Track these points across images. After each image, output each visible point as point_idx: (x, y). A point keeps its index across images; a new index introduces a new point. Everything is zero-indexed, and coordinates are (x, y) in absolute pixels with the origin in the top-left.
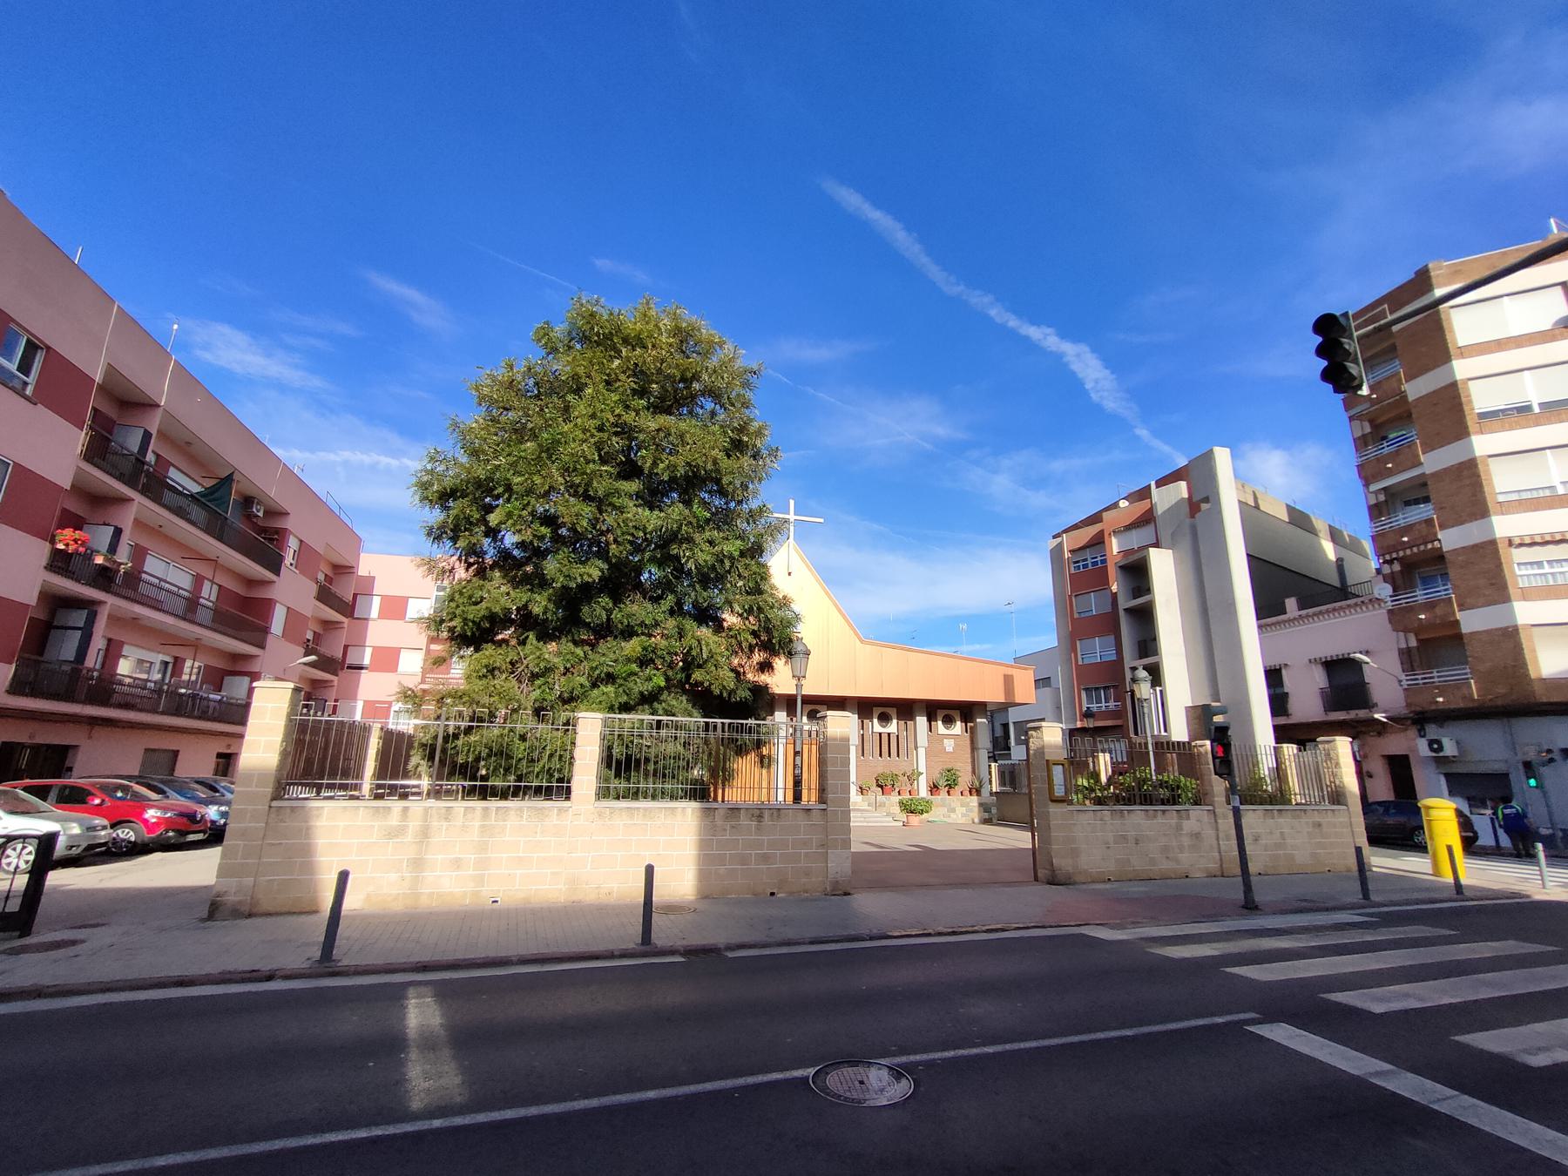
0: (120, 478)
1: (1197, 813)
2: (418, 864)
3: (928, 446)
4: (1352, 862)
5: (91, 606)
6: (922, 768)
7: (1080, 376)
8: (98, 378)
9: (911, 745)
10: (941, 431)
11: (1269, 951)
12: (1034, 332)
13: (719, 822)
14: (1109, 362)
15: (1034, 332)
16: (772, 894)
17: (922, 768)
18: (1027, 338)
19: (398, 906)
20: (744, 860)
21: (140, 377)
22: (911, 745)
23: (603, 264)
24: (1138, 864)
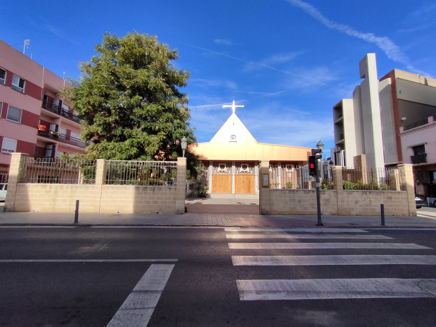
0: (55, 112)
1: (331, 192)
2: (54, 200)
3: (324, 84)
4: (379, 210)
5: (54, 145)
6: (280, 182)
7: (383, 50)
8: (42, 87)
9: (277, 175)
10: (329, 78)
11: (282, 239)
12: (364, 36)
13: (140, 191)
14: (397, 42)
15: (364, 36)
16: (157, 213)
17: (280, 182)
18: (361, 39)
19: (50, 211)
20: (148, 202)
21: (55, 86)
22: (277, 175)
23: (217, 41)
24: (299, 209)
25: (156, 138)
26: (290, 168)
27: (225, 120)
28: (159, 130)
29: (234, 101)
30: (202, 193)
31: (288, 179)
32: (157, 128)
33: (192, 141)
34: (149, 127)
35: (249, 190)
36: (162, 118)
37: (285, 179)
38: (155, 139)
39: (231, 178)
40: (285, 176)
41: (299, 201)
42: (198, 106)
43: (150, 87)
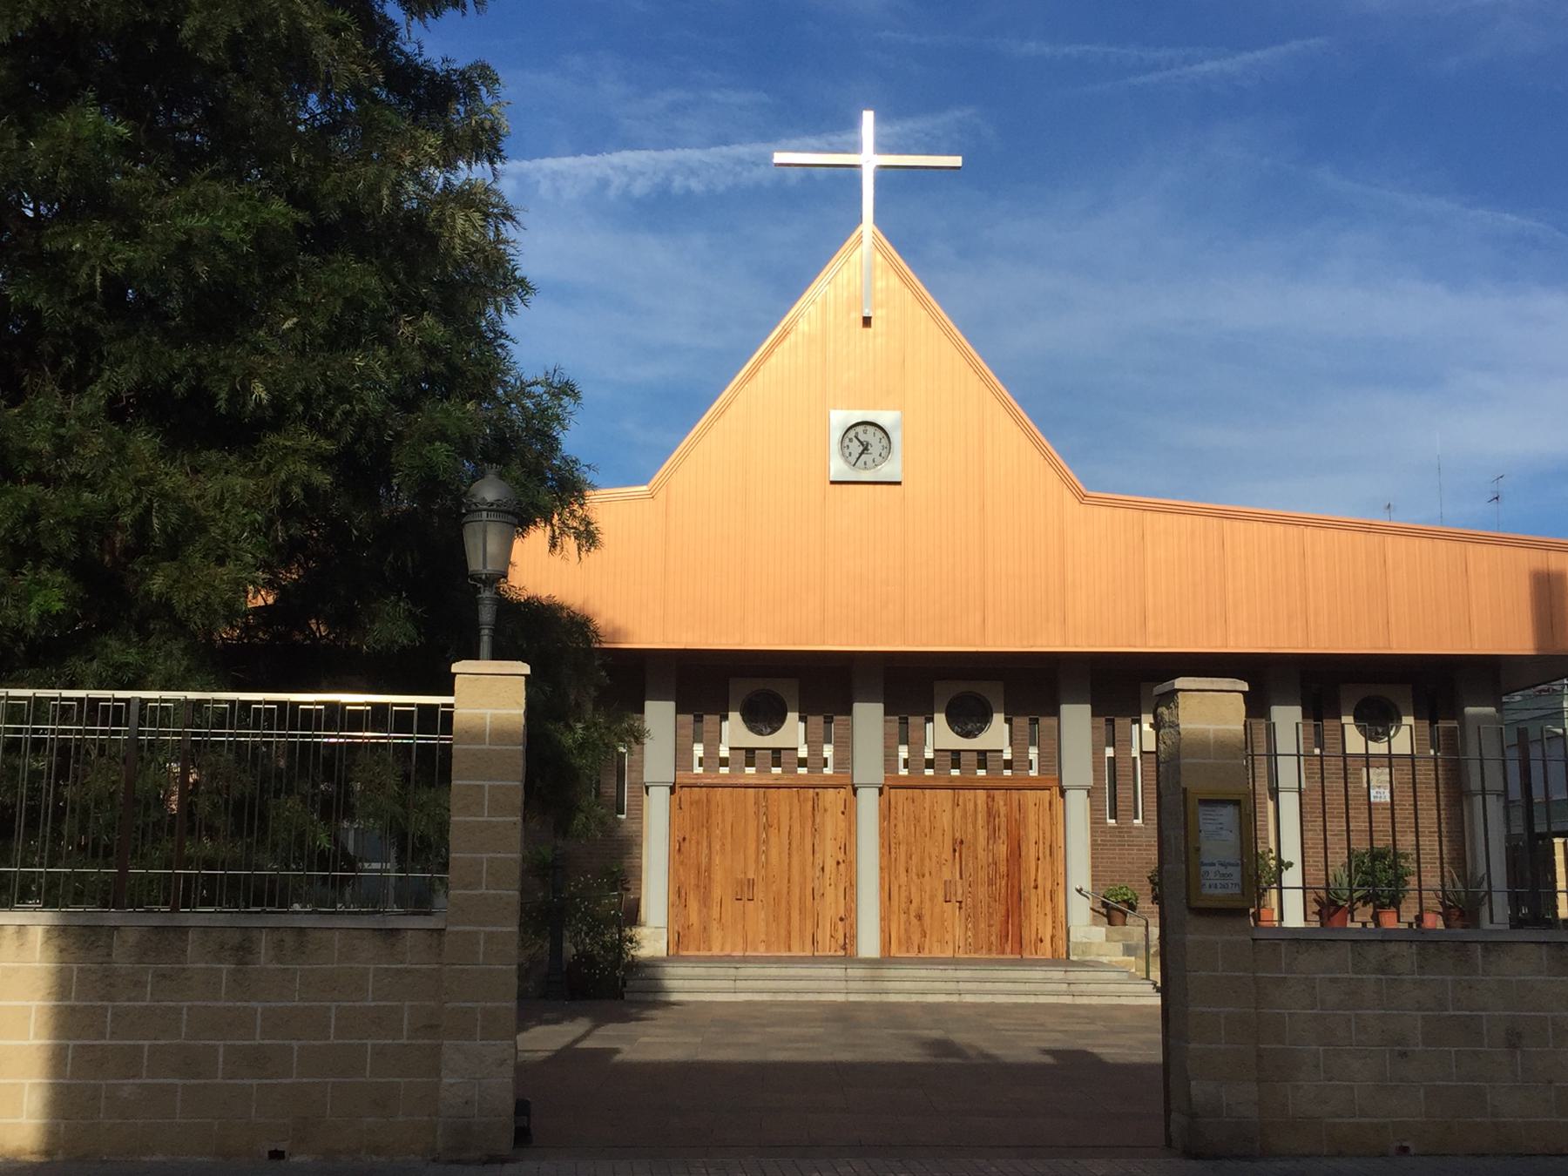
13: (122, 962)
16: (276, 1155)
25: (237, 482)
26: (1377, 720)
27: (791, 282)
28: (277, 416)
29: (868, 117)
30: (586, 958)
31: (1359, 824)
32: (260, 391)
33: (547, 489)
34: (179, 388)
35: (1009, 916)
36: (297, 305)
37: (1336, 825)
38: (224, 487)
39: (849, 812)
40: (1335, 786)
41: (1513, 1040)
42: (549, 164)
43: (203, 34)
